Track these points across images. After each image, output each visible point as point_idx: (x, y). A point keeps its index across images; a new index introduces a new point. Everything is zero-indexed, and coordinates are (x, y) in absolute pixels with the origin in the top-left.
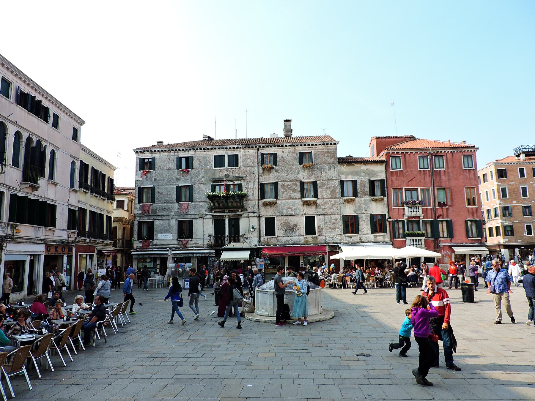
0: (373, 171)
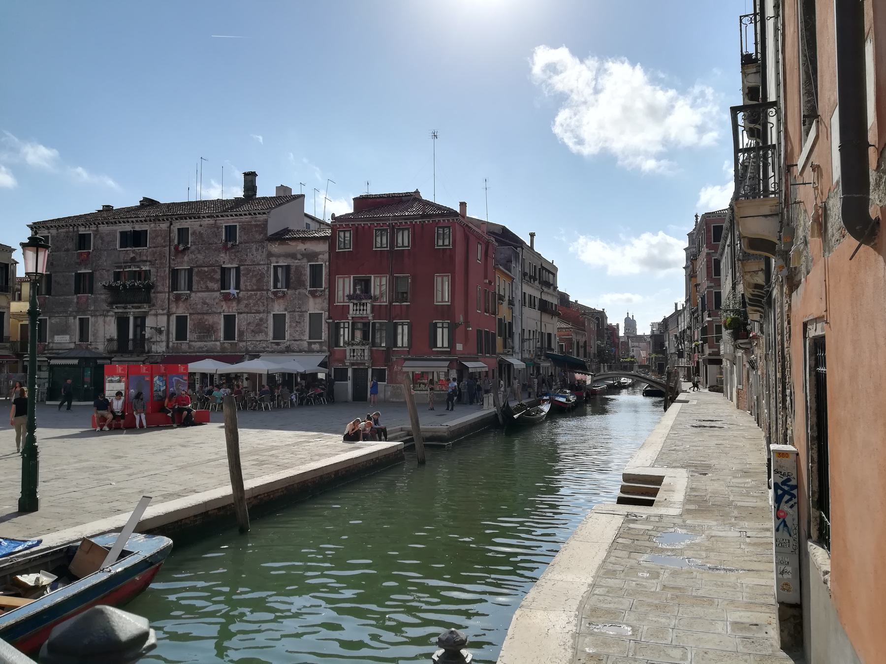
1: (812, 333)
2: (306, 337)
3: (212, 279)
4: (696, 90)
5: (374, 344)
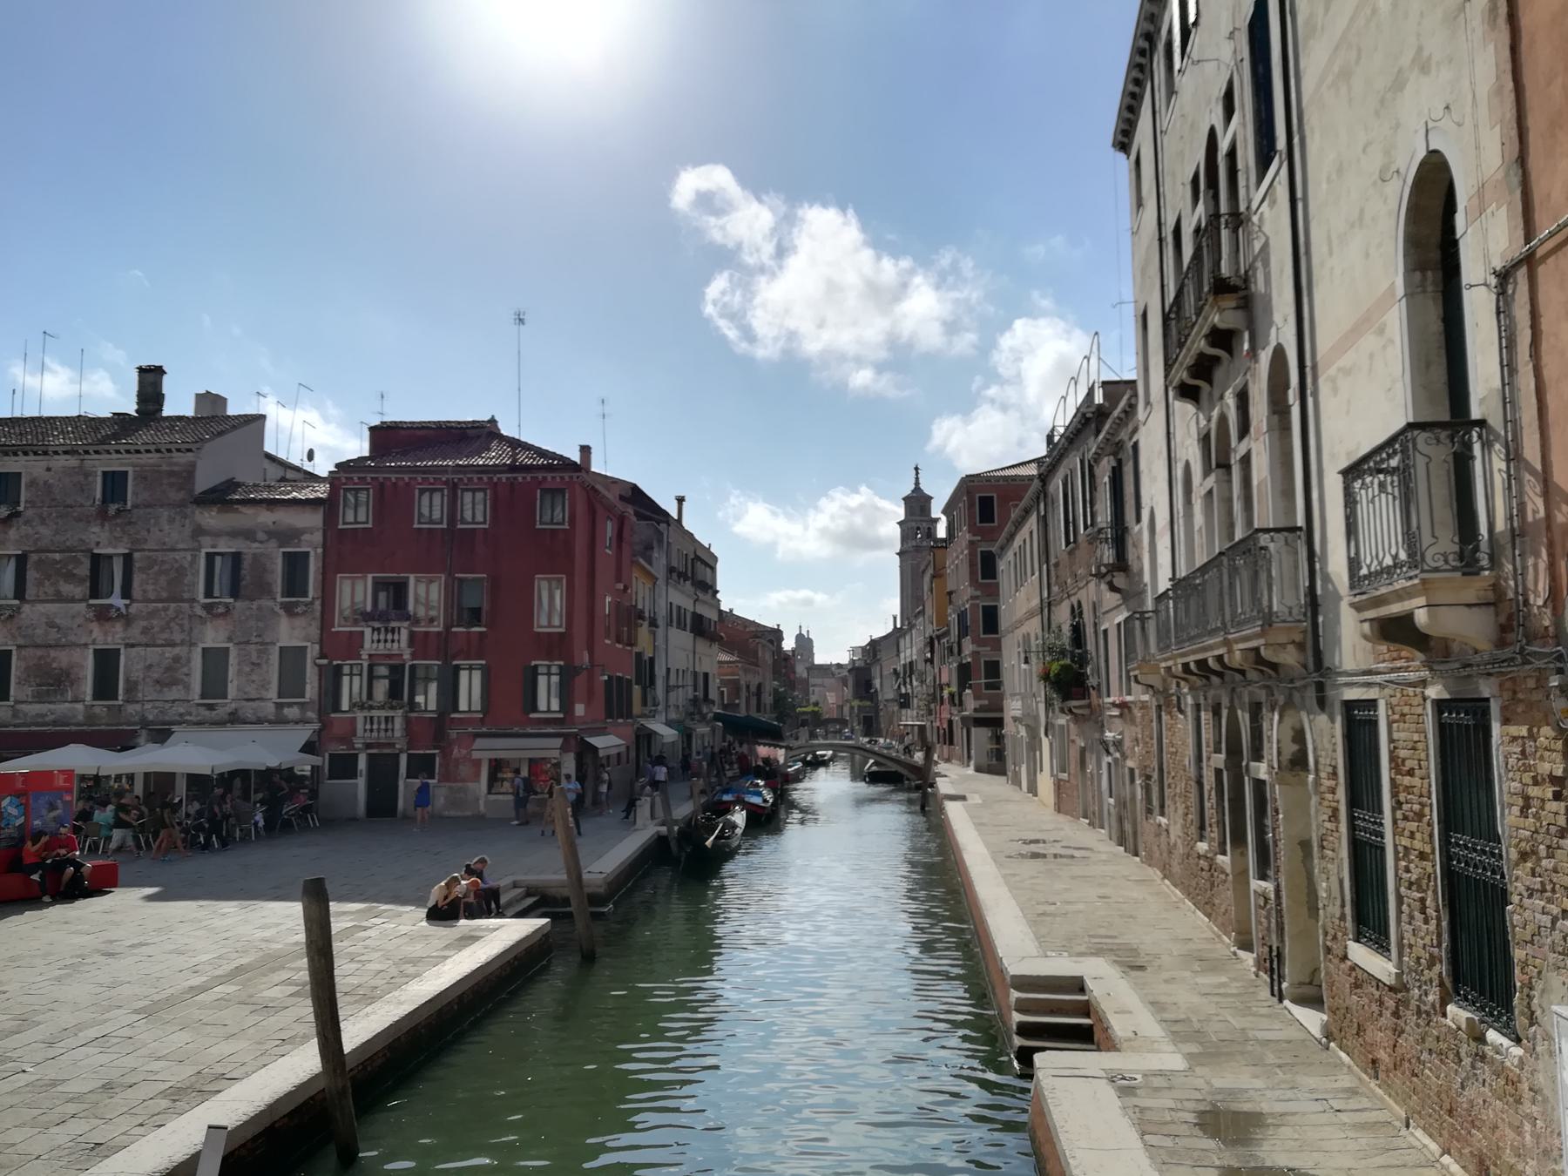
2: (272, 693)
3: (70, 577)
4: (945, 259)
5: (412, 705)
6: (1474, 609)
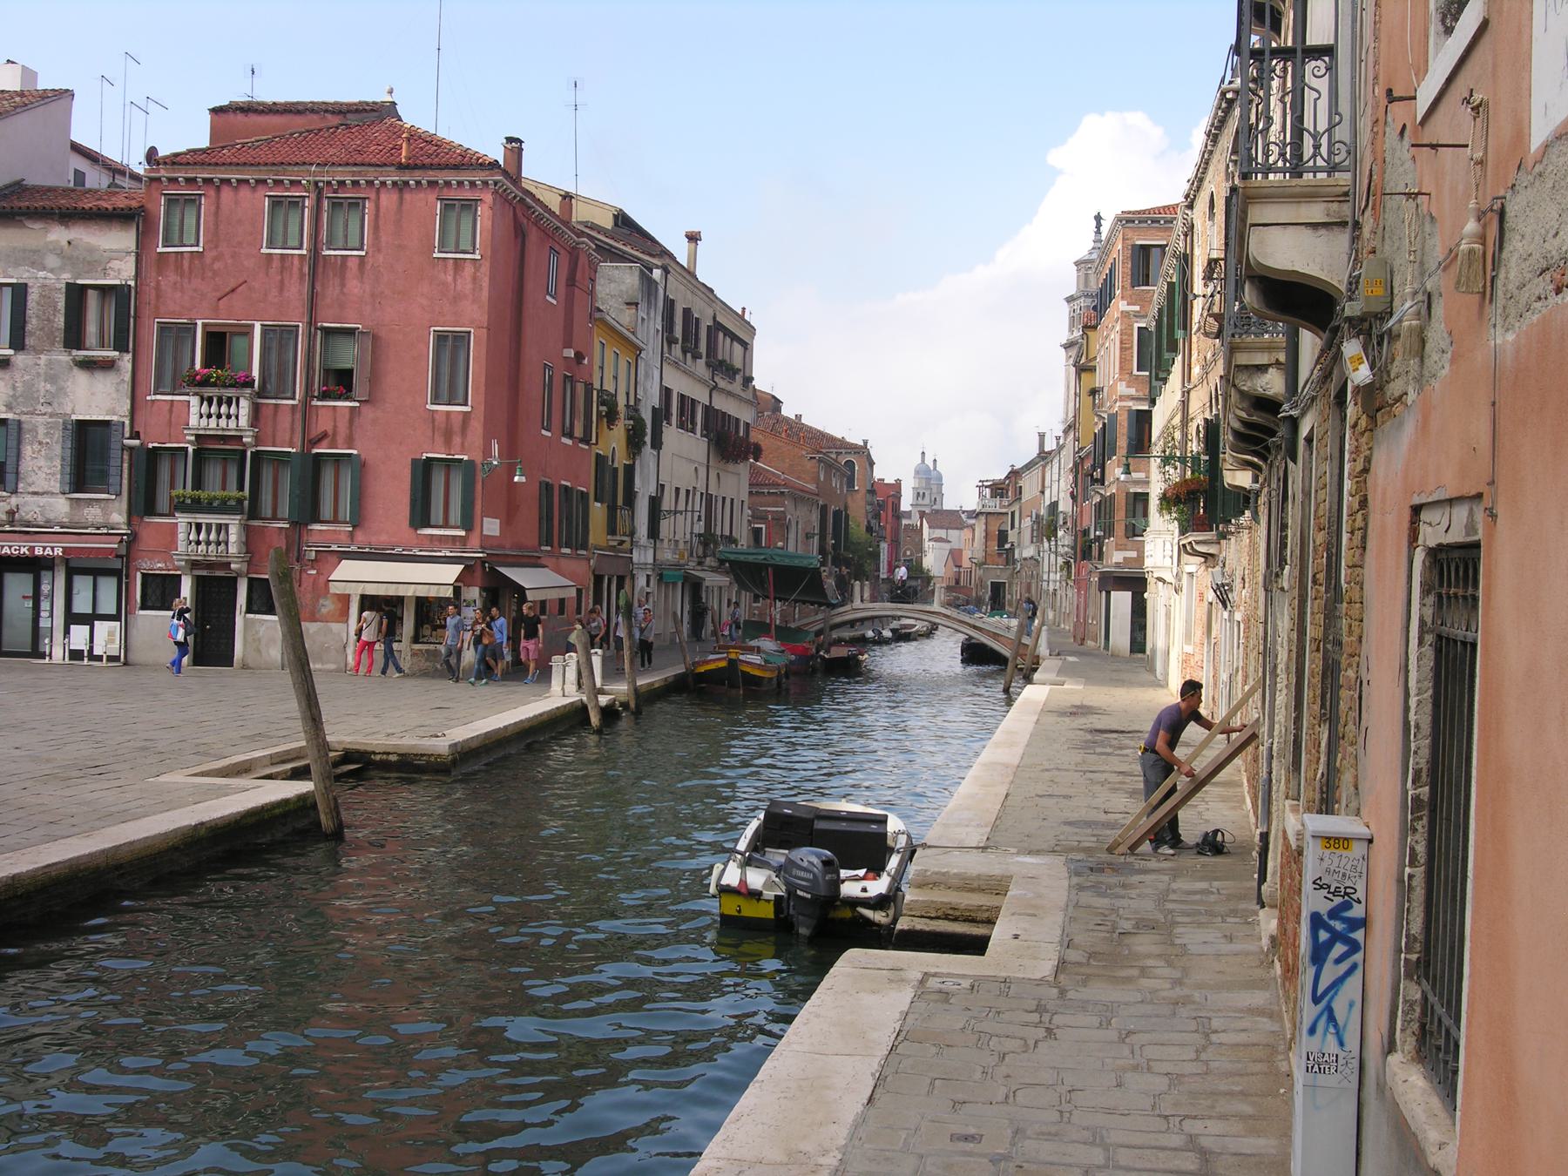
0: (91, 250)
1: (1433, 533)
6: (1323, 231)
